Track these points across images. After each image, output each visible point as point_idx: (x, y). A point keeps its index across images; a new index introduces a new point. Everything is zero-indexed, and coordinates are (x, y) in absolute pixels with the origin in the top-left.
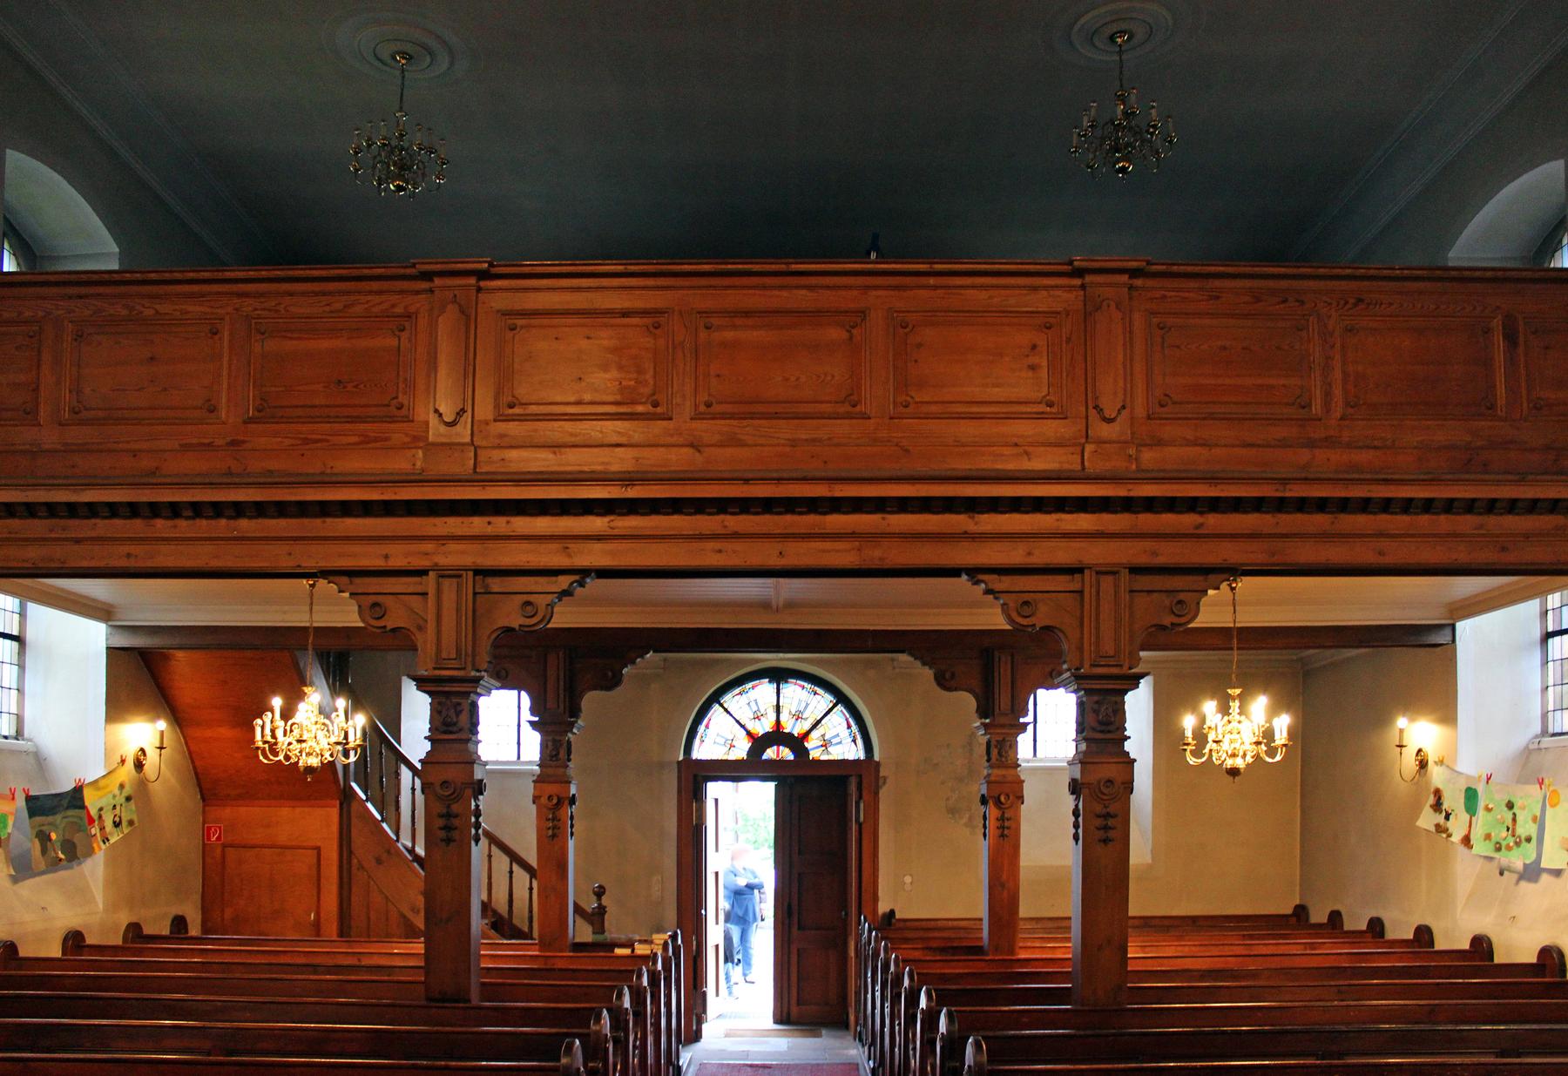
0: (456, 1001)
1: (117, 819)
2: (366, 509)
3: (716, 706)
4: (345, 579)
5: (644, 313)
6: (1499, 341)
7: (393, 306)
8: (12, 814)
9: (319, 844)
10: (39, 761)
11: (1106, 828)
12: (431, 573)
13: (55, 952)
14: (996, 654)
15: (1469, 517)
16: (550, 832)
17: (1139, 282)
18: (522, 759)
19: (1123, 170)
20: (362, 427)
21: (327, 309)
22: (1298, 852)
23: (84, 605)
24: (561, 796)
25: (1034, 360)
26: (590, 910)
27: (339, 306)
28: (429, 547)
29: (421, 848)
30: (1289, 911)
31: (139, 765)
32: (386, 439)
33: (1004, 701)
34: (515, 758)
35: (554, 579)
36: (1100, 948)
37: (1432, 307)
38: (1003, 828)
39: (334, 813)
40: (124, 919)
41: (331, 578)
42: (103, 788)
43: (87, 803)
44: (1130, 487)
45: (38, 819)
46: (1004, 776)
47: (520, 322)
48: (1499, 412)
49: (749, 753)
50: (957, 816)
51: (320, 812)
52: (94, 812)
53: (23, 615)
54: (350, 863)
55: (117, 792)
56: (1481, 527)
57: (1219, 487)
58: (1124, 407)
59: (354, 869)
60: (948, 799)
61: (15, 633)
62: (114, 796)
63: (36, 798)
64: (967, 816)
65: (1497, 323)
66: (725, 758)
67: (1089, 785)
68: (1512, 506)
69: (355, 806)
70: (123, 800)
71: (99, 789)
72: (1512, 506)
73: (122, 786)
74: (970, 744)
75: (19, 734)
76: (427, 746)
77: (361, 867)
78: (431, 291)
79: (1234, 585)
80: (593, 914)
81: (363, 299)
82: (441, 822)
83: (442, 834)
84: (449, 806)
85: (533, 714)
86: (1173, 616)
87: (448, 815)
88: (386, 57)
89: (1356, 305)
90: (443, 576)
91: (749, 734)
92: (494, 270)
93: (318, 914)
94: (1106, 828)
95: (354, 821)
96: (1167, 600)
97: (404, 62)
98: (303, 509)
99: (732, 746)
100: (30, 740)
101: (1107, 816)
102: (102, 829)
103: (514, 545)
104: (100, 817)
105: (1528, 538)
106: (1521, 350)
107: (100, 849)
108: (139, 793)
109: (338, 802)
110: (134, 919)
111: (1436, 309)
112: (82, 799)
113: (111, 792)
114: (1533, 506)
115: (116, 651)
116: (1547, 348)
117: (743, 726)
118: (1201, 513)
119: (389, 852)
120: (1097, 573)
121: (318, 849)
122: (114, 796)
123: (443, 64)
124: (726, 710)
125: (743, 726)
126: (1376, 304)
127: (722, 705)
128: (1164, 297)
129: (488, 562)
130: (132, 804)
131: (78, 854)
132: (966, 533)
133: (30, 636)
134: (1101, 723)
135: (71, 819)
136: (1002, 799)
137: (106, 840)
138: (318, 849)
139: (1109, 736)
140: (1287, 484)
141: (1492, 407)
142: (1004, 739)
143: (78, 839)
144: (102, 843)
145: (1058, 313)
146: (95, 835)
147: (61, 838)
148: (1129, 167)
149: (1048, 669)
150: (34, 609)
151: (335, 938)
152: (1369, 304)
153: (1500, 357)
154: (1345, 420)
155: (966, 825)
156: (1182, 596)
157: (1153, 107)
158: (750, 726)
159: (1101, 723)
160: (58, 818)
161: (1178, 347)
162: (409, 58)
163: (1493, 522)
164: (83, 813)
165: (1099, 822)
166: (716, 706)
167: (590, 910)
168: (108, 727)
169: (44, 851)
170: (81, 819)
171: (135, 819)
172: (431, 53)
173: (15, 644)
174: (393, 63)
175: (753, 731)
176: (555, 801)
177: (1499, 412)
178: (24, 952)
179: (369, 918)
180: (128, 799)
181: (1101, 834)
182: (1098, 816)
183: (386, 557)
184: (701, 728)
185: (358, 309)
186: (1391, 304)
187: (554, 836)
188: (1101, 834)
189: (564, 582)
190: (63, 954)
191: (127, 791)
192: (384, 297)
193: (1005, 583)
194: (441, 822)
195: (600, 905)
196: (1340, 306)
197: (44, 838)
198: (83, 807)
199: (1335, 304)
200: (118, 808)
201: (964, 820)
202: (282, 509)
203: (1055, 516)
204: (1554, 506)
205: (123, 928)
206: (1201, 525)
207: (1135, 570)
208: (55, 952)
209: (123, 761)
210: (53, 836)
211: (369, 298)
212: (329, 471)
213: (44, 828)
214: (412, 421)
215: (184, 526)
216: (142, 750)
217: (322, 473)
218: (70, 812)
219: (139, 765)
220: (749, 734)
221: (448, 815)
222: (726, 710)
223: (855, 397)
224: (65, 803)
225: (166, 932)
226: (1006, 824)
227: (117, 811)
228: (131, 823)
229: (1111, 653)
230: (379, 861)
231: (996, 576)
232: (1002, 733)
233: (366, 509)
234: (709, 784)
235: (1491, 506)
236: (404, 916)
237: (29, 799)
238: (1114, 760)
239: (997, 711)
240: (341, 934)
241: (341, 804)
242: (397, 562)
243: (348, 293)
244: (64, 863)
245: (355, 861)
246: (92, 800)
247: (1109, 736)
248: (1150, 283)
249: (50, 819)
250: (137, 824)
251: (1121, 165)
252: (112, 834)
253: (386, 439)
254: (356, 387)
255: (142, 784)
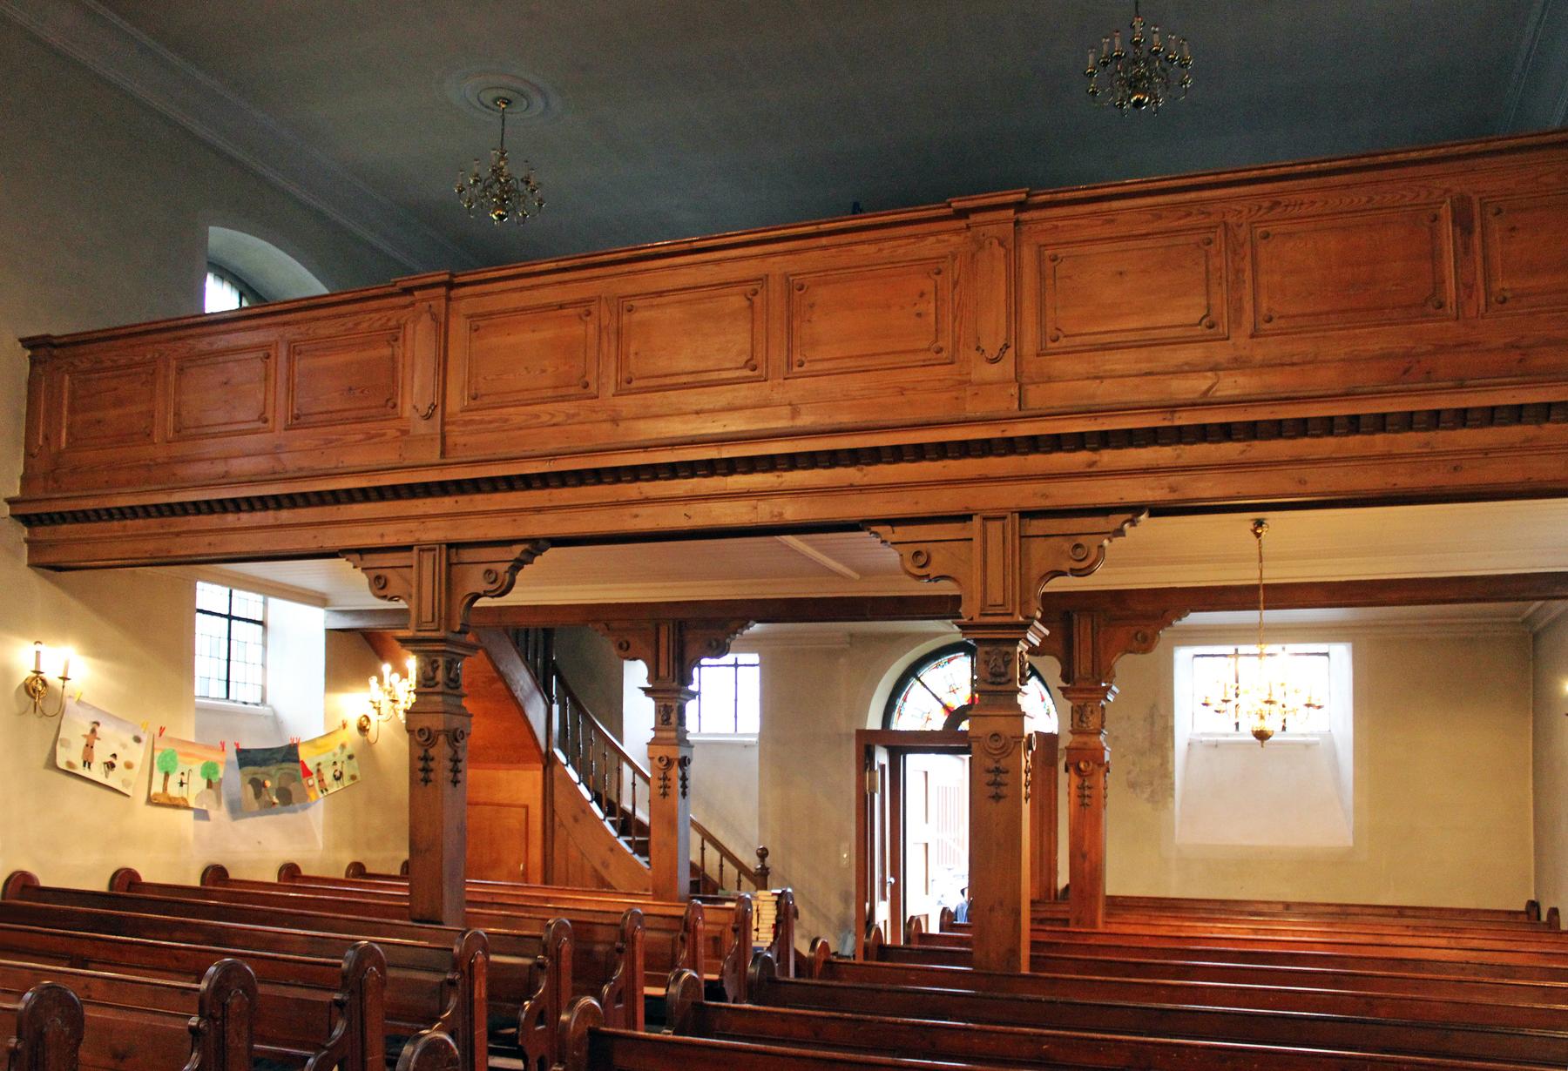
0: (433, 923)
1: (338, 774)
2: (365, 495)
3: (913, 680)
4: (356, 557)
5: (575, 304)
6: (1447, 228)
7: (389, 320)
8: (222, 763)
9: (526, 803)
10: (276, 722)
11: (995, 784)
12: (415, 548)
13: (272, 878)
14: (1075, 617)
15: (1411, 434)
16: (662, 791)
17: (1025, 216)
18: (739, 731)
19: (1139, 103)
20: (364, 425)
21: (344, 328)
22: (1531, 840)
23: (298, 593)
24: (671, 757)
25: (921, 307)
26: (753, 870)
27: (350, 325)
28: (412, 525)
29: (642, 810)
30: (1522, 908)
31: (363, 729)
32: (384, 435)
33: (1083, 665)
34: (733, 731)
35: (507, 549)
36: (991, 909)
37: (1364, 199)
38: (1084, 796)
39: (539, 774)
40: (347, 858)
41: (348, 556)
42: (320, 747)
43: (302, 757)
44: (1003, 427)
45: (250, 769)
46: (1085, 743)
47: (482, 324)
48: (1449, 312)
49: (946, 725)
50: (1138, 791)
51: (529, 774)
52: (311, 766)
53: (265, 604)
54: (553, 819)
55: (337, 750)
56: (1427, 444)
57: (1100, 421)
58: (1007, 346)
59: (556, 827)
60: (1129, 773)
61: (259, 618)
62: (335, 755)
63: (248, 751)
64: (1149, 790)
65: (1445, 211)
66: (923, 729)
67: (978, 738)
68: (1463, 418)
69: (556, 769)
70: (344, 758)
71: (316, 747)
72: (1463, 418)
73: (343, 746)
74: (1152, 716)
75: (263, 701)
76: (413, 697)
77: (562, 825)
78: (412, 304)
79: (1259, 531)
80: (755, 875)
81: (368, 317)
82: (421, 764)
83: (421, 775)
84: (426, 751)
85: (649, 682)
86: (1071, 562)
87: (426, 759)
88: (490, 104)
89: (1271, 208)
90: (423, 550)
91: (945, 707)
92: (456, 280)
93: (526, 867)
94: (995, 784)
95: (556, 783)
96: (1067, 545)
97: (503, 106)
98: (321, 499)
99: (928, 719)
100: (270, 706)
101: (998, 771)
102: (321, 781)
103: (474, 520)
104: (319, 770)
105: (1486, 454)
106: (1476, 240)
107: (318, 798)
108: (365, 752)
109: (541, 766)
110: (358, 859)
111: (1368, 202)
112: (297, 755)
113: (330, 750)
114: (1491, 416)
115: (338, 633)
116: (1513, 229)
117: (939, 700)
118: (1094, 450)
119: (584, 812)
120: (986, 519)
121: (527, 807)
122: (335, 755)
123: (538, 102)
124: (923, 684)
125: (939, 700)
126: (1295, 205)
127: (918, 679)
128: (1056, 227)
129: (456, 536)
130: (354, 761)
131: (294, 800)
132: (851, 485)
133: (270, 623)
134: (994, 675)
135: (286, 771)
136: (1082, 766)
137: (324, 789)
138: (527, 807)
139: (999, 688)
140: (1175, 411)
141: (1441, 306)
142: (1085, 705)
143: (293, 787)
144: (320, 793)
145: (945, 257)
146: (313, 785)
147: (277, 786)
148: (1144, 99)
149: (1133, 632)
150: (272, 601)
151: (539, 885)
152: (1287, 206)
153: (1448, 247)
154: (1257, 337)
155: (1148, 800)
156: (1081, 540)
157: (1155, 32)
158: (946, 701)
159: (994, 675)
160: (272, 769)
161: (1070, 277)
162: (508, 102)
163: (1441, 439)
164: (299, 766)
165: (991, 777)
166: (913, 680)
167: (753, 870)
168: (328, 695)
169: (258, 795)
170: (297, 770)
171: (358, 774)
172: (522, 95)
173: (260, 628)
174: (496, 108)
175: (949, 705)
176: (665, 762)
177: (1449, 312)
178: (232, 876)
179: (567, 870)
180: (350, 757)
181: (992, 790)
182: (988, 771)
183: (382, 536)
184: (899, 702)
185: (365, 325)
186: (1313, 203)
187: (665, 795)
188: (992, 790)
189: (517, 550)
190: (279, 880)
191: (349, 750)
192: (383, 314)
193: (901, 533)
194: (421, 764)
195: (763, 867)
196: (1253, 213)
197: (258, 786)
198: (297, 760)
199: (1246, 212)
200: (339, 764)
201: (1146, 796)
202: (307, 500)
203: (940, 464)
204: (1545, 412)
205: (346, 866)
206: (1094, 463)
207: (1027, 514)
208: (272, 878)
209: (344, 726)
210: (268, 783)
211: (372, 315)
212: (341, 465)
213: (258, 777)
214: (400, 418)
215: (246, 518)
216: (366, 717)
217: (337, 468)
218: (285, 765)
219: (363, 729)
220: (945, 707)
221: (426, 759)
222: (923, 684)
223: (753, 362)
224: (279, 756)
225: (397, 872)
226: (1087, 792)
227: (339, 766)
228: (353, 778)
229: (1000, 601)
230: (576, 820)
231: (888, 528)
232: (1083, 698)
233: (365, 495)
234: (909, 757)
235: (1435, 420)
236: (596, 871)
237: (240, 752)
238: (1003, 713)
239: (1077, 675)
240: (545, 882)
241: (545, 768)
242: (390, 540)
243: (356, 313)
244: (278, 806)
245: (557, 819)
246: (304, 753)
247: (999, 688)
248: (1035, 214)
249: (263, 769)
250: (359, 778)
251: (1135, 98)
252: (332, 786)
253: (384, 435)
254: (362, 392)
255: (368, 747)
